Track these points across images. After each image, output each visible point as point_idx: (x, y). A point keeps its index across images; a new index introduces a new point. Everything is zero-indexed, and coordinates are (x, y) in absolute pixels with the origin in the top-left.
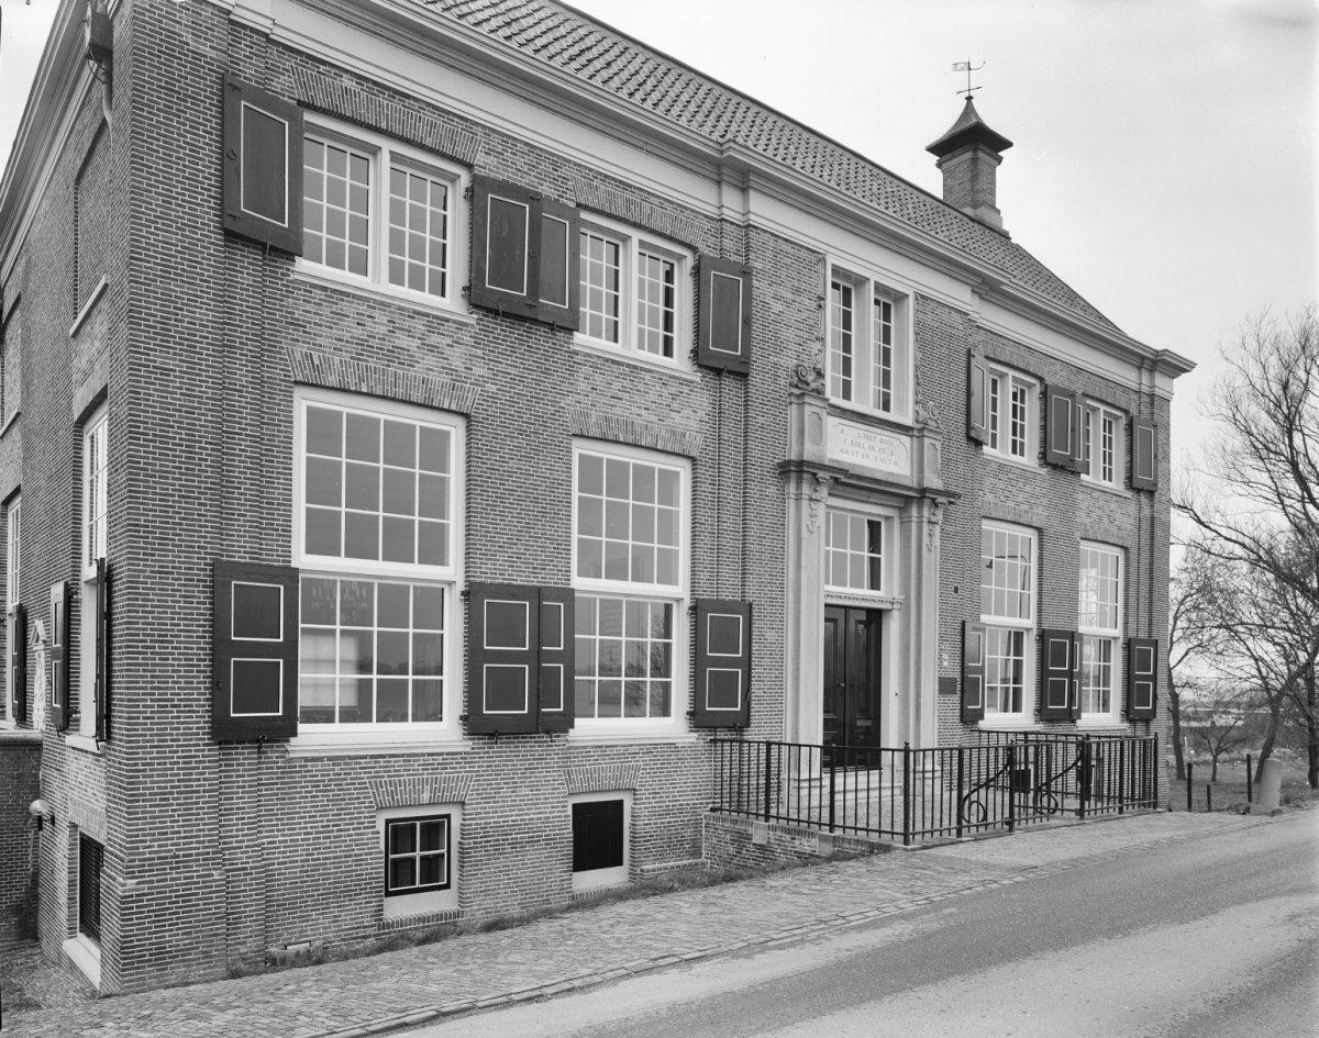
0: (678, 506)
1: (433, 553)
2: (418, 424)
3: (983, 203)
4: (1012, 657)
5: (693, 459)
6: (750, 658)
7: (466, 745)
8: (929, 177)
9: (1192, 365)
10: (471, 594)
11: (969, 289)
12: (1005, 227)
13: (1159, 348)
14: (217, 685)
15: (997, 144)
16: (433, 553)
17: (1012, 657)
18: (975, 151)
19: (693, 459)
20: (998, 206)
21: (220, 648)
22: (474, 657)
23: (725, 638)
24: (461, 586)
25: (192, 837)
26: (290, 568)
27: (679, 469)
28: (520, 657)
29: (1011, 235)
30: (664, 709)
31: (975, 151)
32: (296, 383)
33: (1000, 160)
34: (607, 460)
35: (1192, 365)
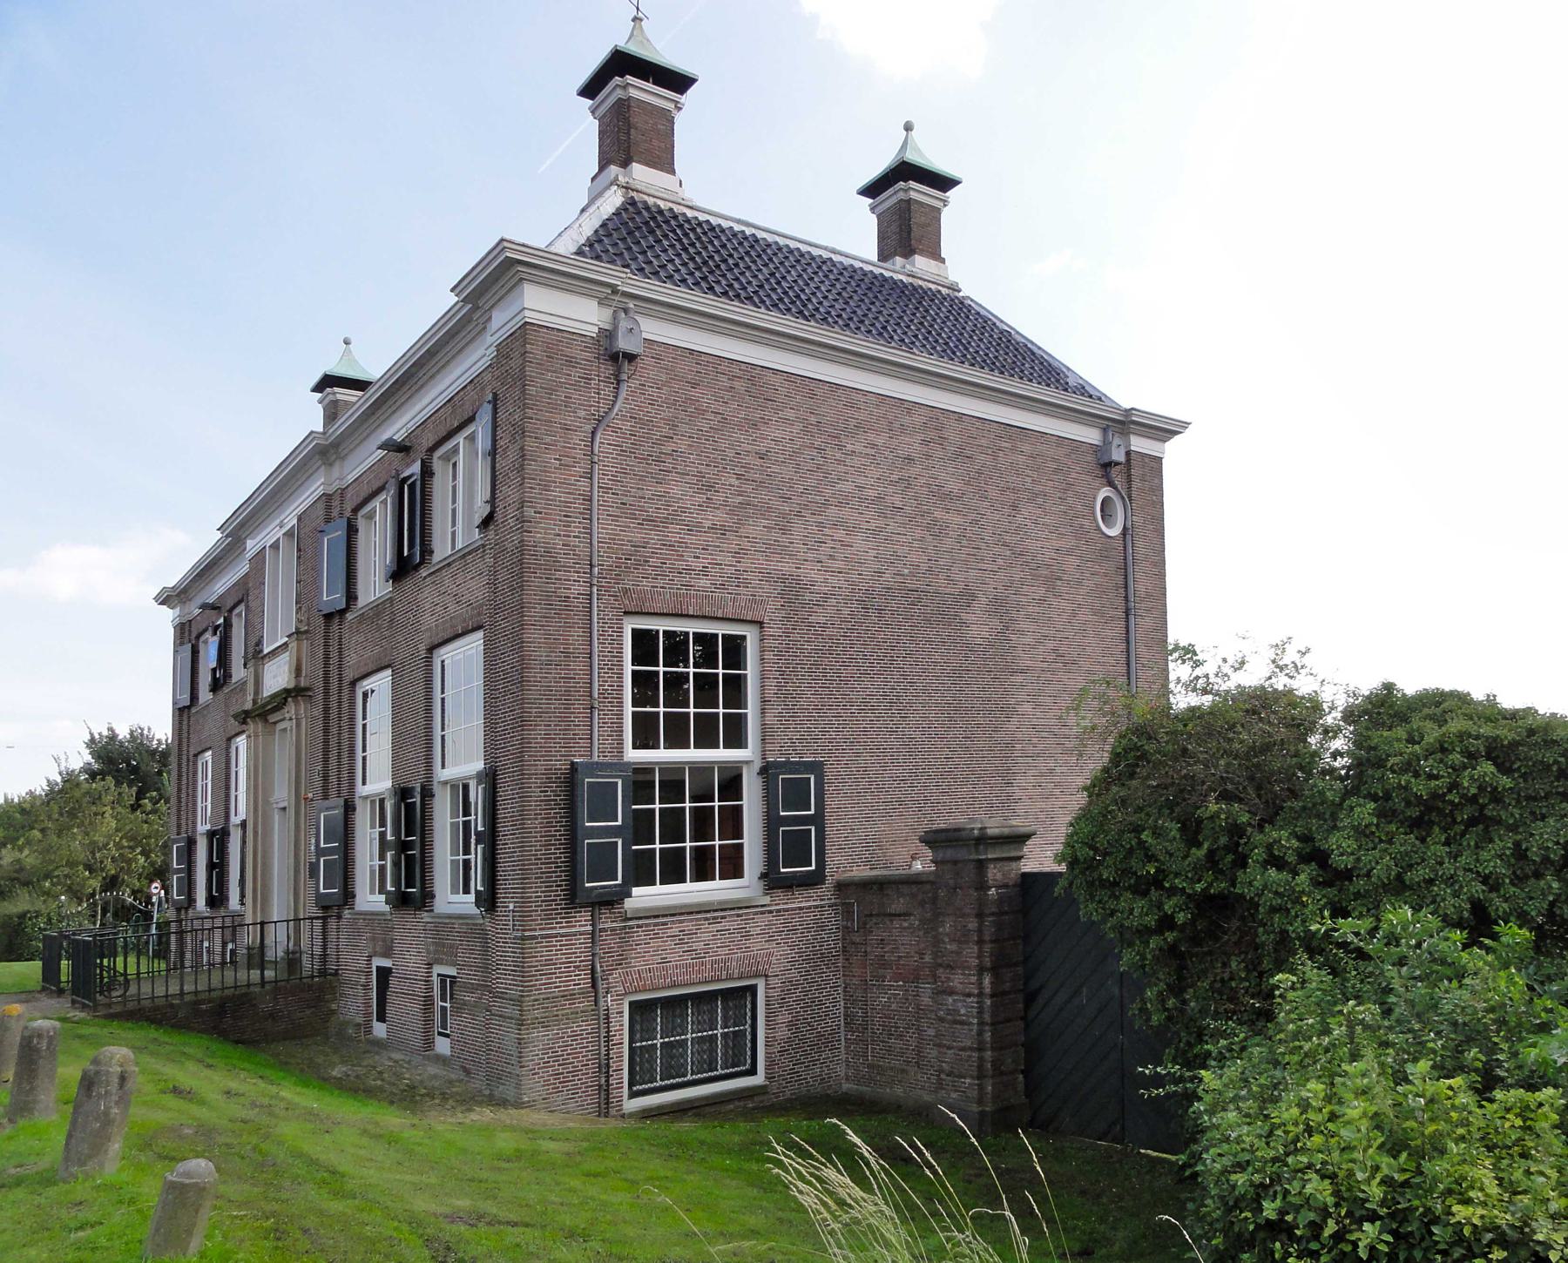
0: (745, 669)
1: (736, 738)
2: (720, 633)
4: (378, 829)
5: (760, 624)
9: (1185, 425)
10: (766, 771)
11: (594, 303)
13: (1126, 405)
17: (378, 829)
19: (760, 624)
20: (943, 256)
22: (772, 822)
23: (797, 795)
24: (757, 765)
25: (545, 984)
28: (615, 832)
30: (733, 867)
32: (625, 613)
34: (694, 633)
35: (1185, 425)
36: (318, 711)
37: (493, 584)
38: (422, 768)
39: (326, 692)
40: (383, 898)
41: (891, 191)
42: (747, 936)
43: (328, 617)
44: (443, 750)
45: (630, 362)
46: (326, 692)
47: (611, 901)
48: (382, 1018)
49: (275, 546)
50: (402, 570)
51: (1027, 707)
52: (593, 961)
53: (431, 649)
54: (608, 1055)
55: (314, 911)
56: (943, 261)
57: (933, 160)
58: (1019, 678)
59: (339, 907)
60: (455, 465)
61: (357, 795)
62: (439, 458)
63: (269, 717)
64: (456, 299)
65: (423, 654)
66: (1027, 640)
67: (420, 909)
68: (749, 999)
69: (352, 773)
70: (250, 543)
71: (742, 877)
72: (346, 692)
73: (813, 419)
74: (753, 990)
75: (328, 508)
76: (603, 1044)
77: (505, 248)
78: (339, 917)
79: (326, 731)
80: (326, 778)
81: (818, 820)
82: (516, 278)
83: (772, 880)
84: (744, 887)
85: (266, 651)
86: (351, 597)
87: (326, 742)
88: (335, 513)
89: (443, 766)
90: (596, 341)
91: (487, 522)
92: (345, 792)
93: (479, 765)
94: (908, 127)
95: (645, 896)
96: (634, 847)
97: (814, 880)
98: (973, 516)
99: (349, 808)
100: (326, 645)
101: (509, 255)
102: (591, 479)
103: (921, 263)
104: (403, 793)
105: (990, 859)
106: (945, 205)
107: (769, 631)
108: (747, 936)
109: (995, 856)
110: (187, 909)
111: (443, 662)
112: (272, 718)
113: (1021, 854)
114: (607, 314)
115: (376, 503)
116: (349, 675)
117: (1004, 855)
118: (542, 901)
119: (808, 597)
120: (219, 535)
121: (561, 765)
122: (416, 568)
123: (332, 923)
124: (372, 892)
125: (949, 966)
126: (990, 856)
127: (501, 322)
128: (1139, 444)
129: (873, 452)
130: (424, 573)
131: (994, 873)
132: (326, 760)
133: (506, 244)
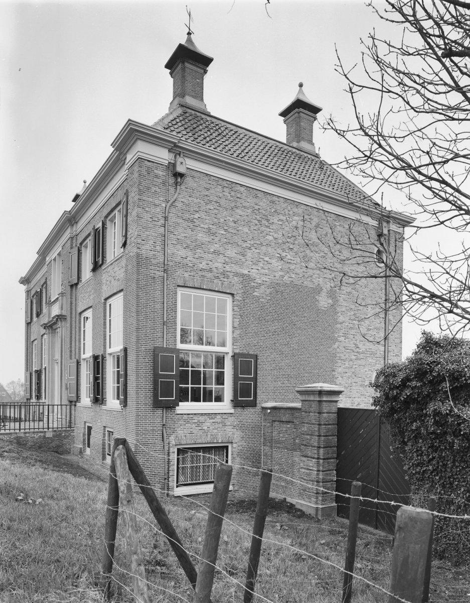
3: (303, 139)
5: (232, 295)
6: (256, 377)
7: (232, 411)
8: (278, 131)
10: (234, 357)
12: (208, 110)
14: (155, 389)
15: (205, 61)
16: (223, 344)
18: (183, 63)
19: (232, 295)
20: (313, 142)
21: (156, 376)
22: (236, 378)
24: (231, 354)
26: (175, 349)
27: (226, 298)
29: (320, 156)
31: (183, 63)
32: (178, 286)
33: (206, 72)
36: (68, 325)
37: (126, 271)
38: (102, 347)
39: (71, 317)
40: (118, 402)
41: (292, 113)
42: (225, 425)
43: (72, 286)
44: (110, 341)
45: (181, 178)
46: (71, 317)
47: (171, 406)
48: (89, 446)
49: (55, 259)
50: (96, 267)
51: (342, 339)
52: (163, 430)
53: (106, 299)
54: (168, 469)
55: (67, 403)
56: (313, 144)
57: (310, 100)
58: (339, 326)
59: (75, 402)
60: (115, 223)
61: (82, 358)
62: (109, 220)
63: (53, 326)
64: (113, 149)
65: (103, 301)
66: (344, 309)
67: (101, 404)
68: (225, 451)
69: (80, 349)
70: (47, 259)
71: (223, 401)
72: (78, 316)
73: (257, 207)
74: (227, 447)
75: (72, 242)
76: (166, 463)
77: (130, 124)
78: (75, 405)
79: (71, 333)
80: (71, 351)
81: (255, 379)
82: (135, 138)
83: (236, 403)
84: (225, 406)
85: (52, 301)
86: (79, 278)
87: (71, 337)
88: (74, 245)
89: (110, 347)
90: (168, 167)
91: (124, 245)
92: (77, 357)
93: (122, 347)
94: (301, 85)
95: (185, 407)
96: (180, 386)
97: (253, 404)
98: (322, 254)
99: (78, 363)
100: (71, 298)
101: (132, 127)
102: (165, 227)
103: (304, 145)
104: (95, 358)
105: (324, 401)
106: (315, 120)
107: (237, 298)
108: (225, 425)
109: (326, 399)
110: (30, 399)
111: (110, 305)
112: (54, 327)
113: (338, 399)
114: (172, 156)
115: (88, 240)
116: (79, 310)
117: (329, 399)
118: (143, 404)
119: (253, 284)
120: (37, 256)
121: (150, 346)
122: (101, 266)
123: (73, 407)
124: (114, 399)
125: (305, 445)
126: (324, 399)
127: (130, 157)
128: (393, 227)
129: (281, 223)
130: (103, 267)
131: (325, 408)
132: (71, 344)
133: (131, 122)
